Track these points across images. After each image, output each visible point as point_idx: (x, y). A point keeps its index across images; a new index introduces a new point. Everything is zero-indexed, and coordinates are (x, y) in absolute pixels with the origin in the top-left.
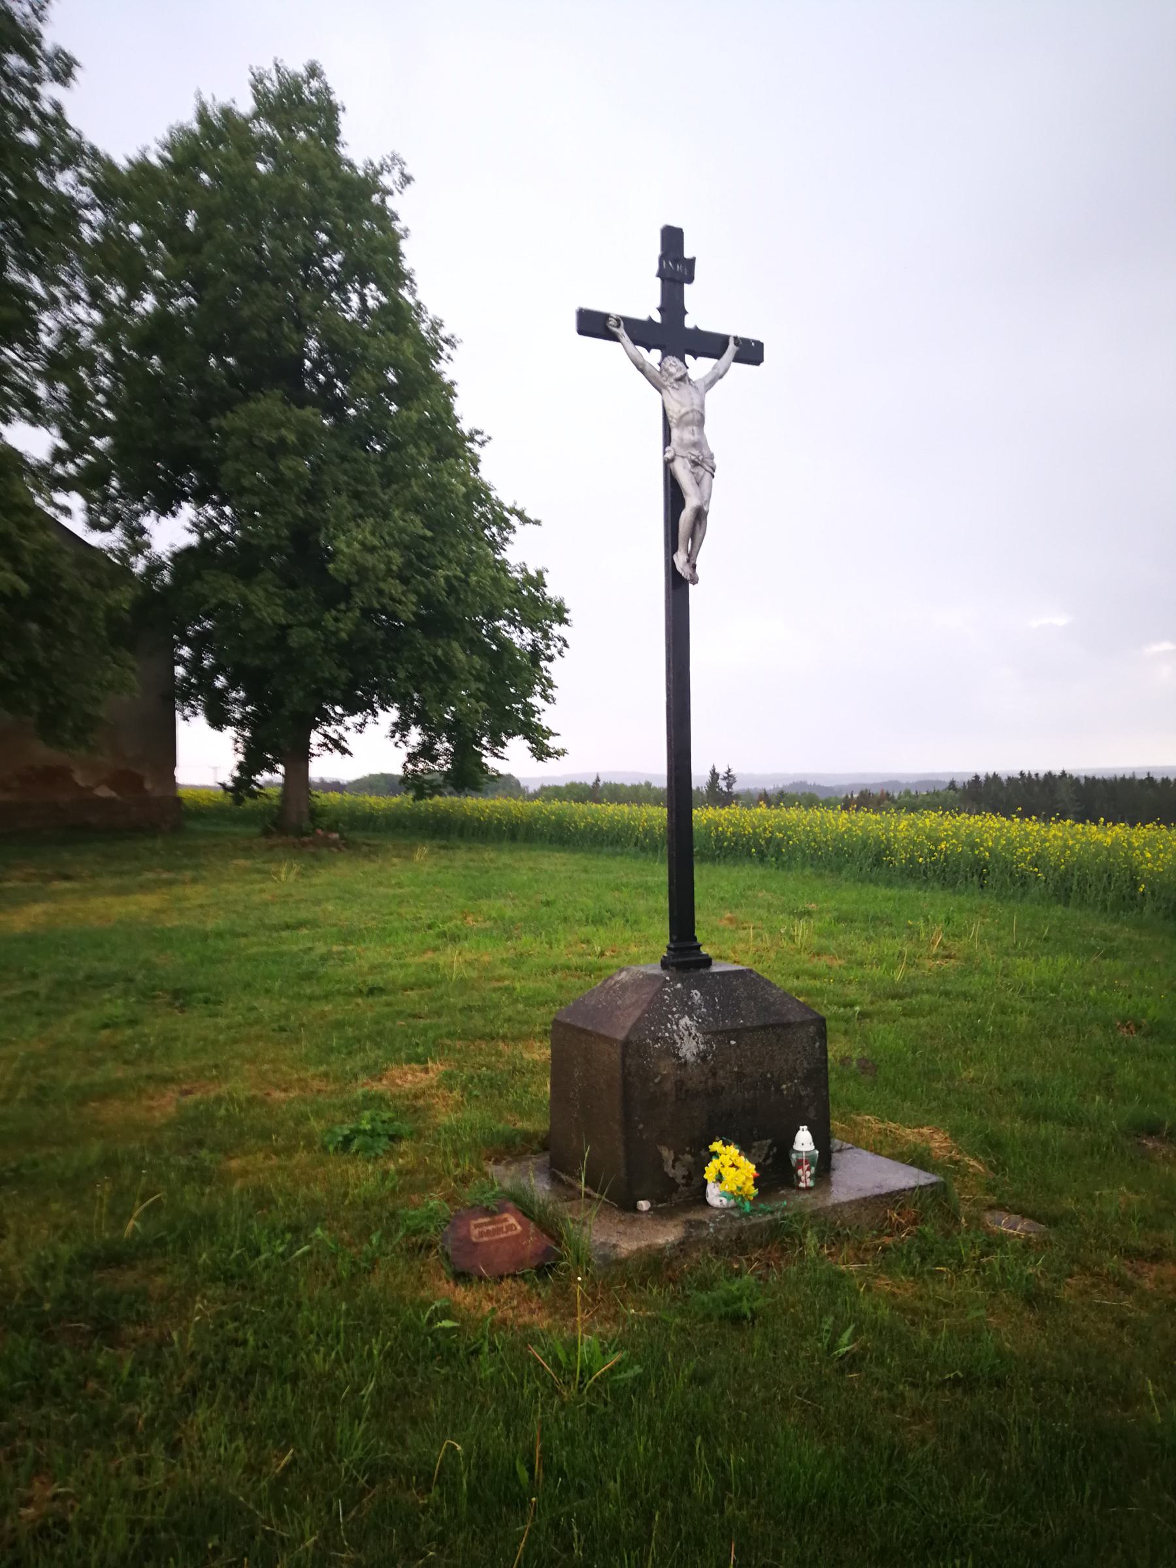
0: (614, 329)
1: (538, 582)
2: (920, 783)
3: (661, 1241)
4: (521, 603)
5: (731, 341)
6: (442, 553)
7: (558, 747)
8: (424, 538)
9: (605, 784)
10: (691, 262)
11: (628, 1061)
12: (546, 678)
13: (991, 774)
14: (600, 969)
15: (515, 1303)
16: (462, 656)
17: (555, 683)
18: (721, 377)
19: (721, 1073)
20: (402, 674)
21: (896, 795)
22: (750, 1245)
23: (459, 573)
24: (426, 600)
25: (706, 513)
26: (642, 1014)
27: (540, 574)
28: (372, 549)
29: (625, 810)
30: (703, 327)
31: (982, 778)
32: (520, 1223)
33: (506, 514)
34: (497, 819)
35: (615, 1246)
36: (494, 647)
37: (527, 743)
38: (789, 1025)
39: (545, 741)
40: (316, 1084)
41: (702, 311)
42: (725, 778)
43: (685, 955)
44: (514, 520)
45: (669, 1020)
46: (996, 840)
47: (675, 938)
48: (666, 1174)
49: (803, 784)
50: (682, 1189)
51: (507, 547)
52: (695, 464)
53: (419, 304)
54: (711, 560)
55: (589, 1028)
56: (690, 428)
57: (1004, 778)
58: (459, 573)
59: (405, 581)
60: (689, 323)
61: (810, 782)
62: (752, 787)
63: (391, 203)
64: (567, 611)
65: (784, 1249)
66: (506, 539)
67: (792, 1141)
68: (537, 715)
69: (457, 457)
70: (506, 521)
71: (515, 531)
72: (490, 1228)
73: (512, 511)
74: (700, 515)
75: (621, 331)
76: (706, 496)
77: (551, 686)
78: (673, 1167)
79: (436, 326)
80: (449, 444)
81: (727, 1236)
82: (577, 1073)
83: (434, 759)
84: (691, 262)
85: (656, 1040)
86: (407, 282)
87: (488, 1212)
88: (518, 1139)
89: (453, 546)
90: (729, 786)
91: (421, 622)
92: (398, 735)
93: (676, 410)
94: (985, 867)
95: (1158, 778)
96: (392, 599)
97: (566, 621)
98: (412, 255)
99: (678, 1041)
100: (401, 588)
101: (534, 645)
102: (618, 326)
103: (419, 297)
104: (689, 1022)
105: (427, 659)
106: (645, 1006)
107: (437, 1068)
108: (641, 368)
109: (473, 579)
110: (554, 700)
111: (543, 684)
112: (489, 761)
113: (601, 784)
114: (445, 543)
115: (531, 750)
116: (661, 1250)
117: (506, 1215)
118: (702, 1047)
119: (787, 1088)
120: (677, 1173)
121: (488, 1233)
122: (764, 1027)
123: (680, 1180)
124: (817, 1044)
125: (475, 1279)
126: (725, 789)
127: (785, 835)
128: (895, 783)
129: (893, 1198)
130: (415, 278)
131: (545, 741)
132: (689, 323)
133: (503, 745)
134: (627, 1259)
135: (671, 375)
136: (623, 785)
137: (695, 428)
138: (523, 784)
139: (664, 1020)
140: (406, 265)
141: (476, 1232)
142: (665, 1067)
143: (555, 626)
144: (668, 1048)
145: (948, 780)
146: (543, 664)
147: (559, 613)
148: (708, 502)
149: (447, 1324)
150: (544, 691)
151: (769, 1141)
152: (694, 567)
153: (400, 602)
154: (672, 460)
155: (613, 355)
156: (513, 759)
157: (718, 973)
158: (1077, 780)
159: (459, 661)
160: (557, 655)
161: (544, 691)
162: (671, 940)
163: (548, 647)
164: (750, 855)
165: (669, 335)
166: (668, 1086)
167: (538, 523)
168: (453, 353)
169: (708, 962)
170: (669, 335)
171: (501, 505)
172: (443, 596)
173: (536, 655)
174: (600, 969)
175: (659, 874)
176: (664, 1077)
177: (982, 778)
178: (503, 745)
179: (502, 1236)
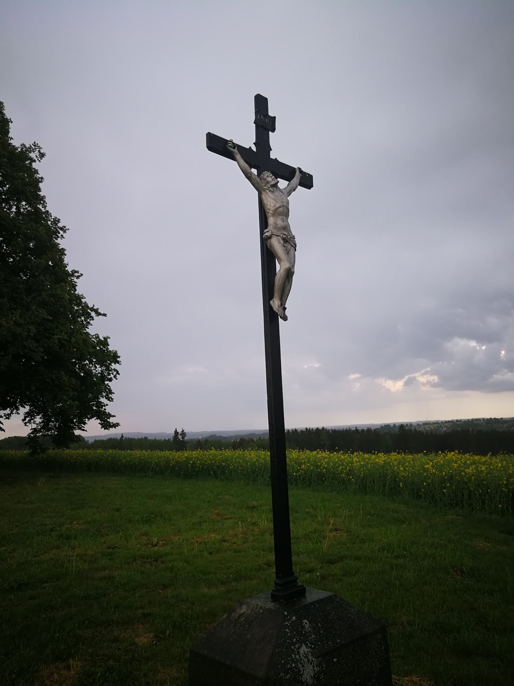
1: (105, 343)
4: (96, 354)
5: (298, 173)
8: (48, 320)
9: (126, 438)
12: (108, 389)
13: (294, 429)
14: (161, 556)
17: (113, 391)
18: (294, 190)
21: (255, 439)
23: (66, 337)
25: (293, 273)
27: (106, 339)
28: (20, 325)
29: (145, 453)
31: (291, 431)
36: (82, 374)
37: (99, 421)
39: (108, 420)
41: (281, 149)
42: (181, 435)
44: (93, 314)
51: (89, 327)
52: (285, 240)
53: (47, 211)
56: (281, 217)
57: (299, 431)
58: (66, 337)
60: (273, 156)
62: (192, 438)
63: (34, 165)
64: (119, 357)
66: (89, 323)
68: (104, 407)
69: (66, 283)
71: (93, 319)
73: (92, 309)
74: (289, 274)
76: (292, 261)
90: (183, 438)
92: (28, 419)
93: (272, 205)
94: (324, 476)
95: (360, 429)
97: (118, 362)
98: (45, 189)
101: (102, 373)
102: (234, 148)
103: (47, 209)
104: (306, 650)
105: (47, 380)
108: (249, 176)
109: (73, 340)
110: (112, 399)
111: (107, 392)
113: (124, 438)
115: (101, 424)
118: (316, 669)
126: (181, 439)
127: (226, 463)
130: (46, 200)
131: (108, 420)
132: (273, 155)
133: (85, 423)
135: (268, 182)
136: (134, 439)
137: (284, 218)
138: (86, 439)
143: (113, 364)
147: (115, 358)
152: (285, 309)
153: (35, 351)
154: (270, 237)
155: (231, 169)
156: (92, 429)
158: (329, 431)
160: (114, 379)
162: (277, 577)
163: (109, 374)
164: (210, 474)
167: (105, 315)
168: (65, 235)
169: (302, 592)
170: (259, 162)
171: (87, 306)
173: (103, 378)
174: (161, 556)
177: (291, 431)
178: (85, 423)
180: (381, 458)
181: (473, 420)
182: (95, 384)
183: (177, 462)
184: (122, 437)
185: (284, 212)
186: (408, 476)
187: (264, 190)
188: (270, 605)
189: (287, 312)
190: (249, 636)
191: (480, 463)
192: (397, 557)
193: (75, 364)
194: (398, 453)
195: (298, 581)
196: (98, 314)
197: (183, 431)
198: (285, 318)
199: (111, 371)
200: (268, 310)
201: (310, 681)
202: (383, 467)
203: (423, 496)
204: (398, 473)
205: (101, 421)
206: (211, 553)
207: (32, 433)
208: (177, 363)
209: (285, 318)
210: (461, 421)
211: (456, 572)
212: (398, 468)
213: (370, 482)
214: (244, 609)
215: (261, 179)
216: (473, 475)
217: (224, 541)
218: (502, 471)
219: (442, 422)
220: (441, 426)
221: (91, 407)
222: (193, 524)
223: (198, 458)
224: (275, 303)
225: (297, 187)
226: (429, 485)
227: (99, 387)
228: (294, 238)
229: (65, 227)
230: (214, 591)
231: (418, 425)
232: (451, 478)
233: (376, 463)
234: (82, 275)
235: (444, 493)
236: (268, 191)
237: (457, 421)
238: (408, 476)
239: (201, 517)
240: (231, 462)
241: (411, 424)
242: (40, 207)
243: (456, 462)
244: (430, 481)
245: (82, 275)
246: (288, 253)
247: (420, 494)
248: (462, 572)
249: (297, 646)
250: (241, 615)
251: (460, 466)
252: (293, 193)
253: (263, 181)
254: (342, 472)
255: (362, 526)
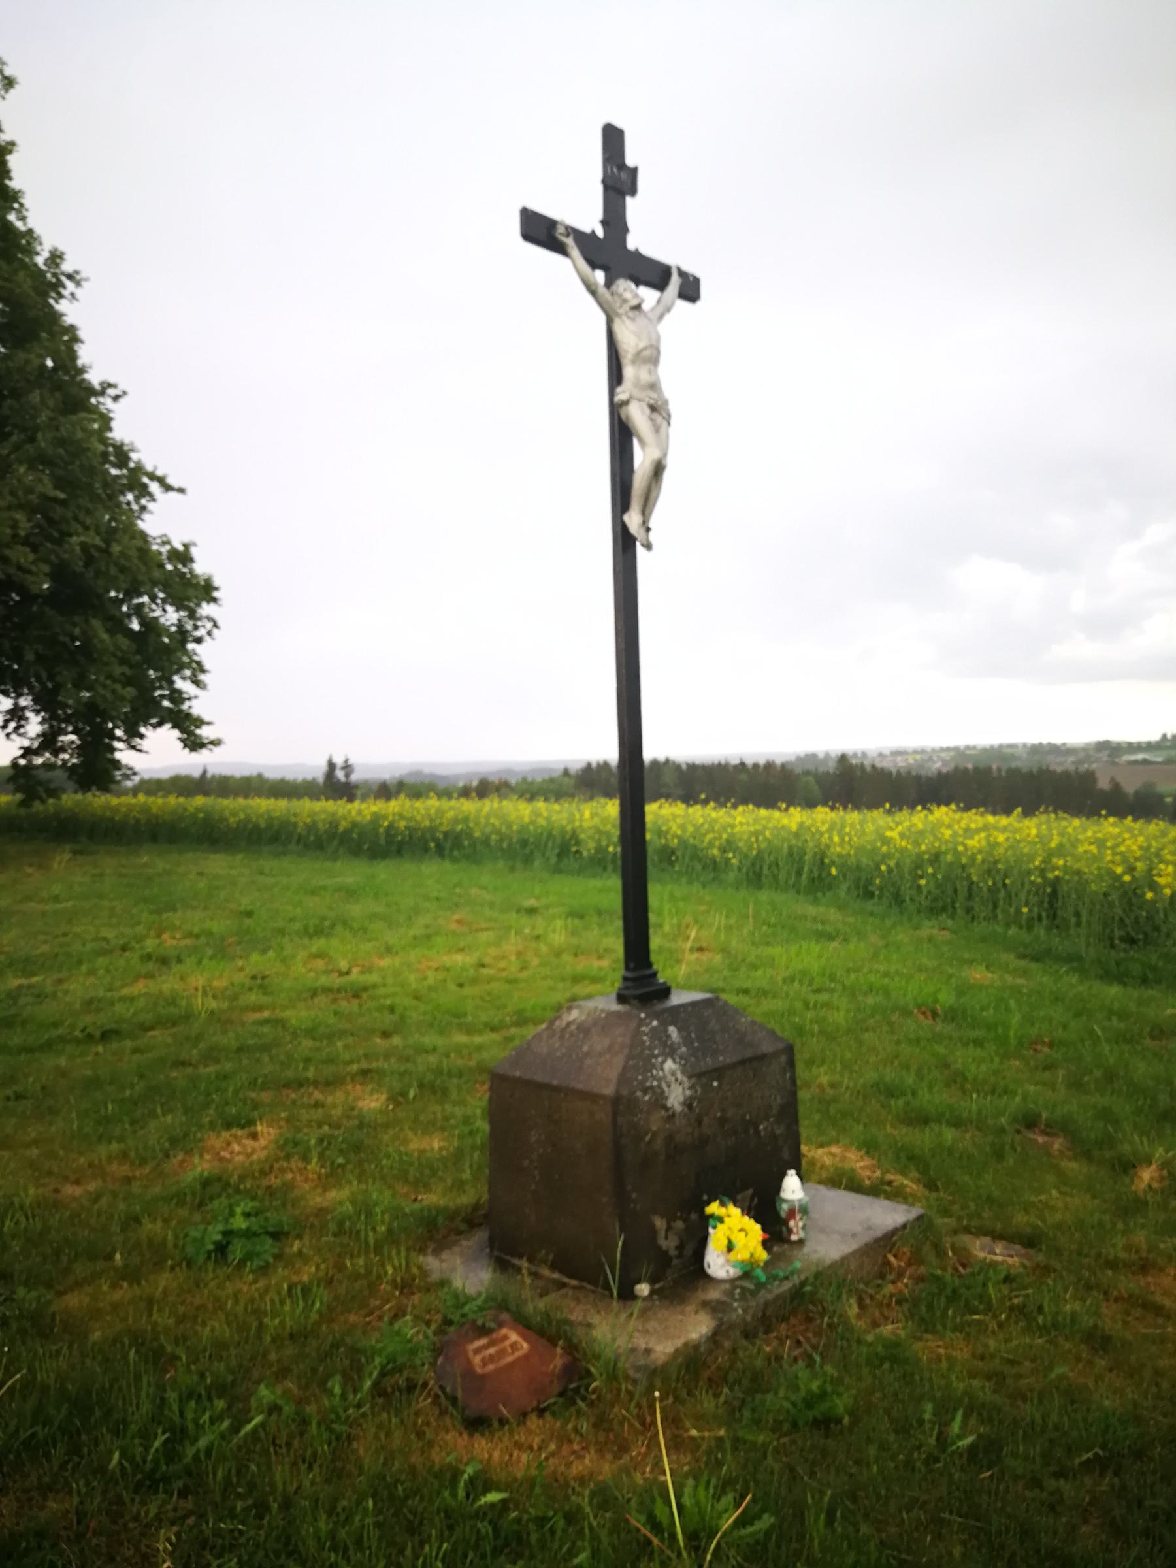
0: (563, 239)
1: (183, 556)
2: (533, 771)
3: (694, 1336)
6: (76, 519)
7: (213, 737)
8: (55, 500)
9: (213, 776)
10: (634, 171)
11: (620, 1120)
13: (601, 762)
15: (553, 1447)
16: (105, 636)
19: (706, 1120)
20: (30, 656)
22: (774, 1320)
23: (98, 541)
24: (60, 573)
26: (626, 1062)
27: (186, 546)
30: (647, 251)
32: (525, 1339)
33: (145, 480)
34: (134, 817)
35: (648, 1351)
37: (176, 733)
38: (762, 1058)
40: (119, 1169)
41: (644, 236)
43: (642, 985)
44: (154, 487)
45: (654, 1066)
46: (683, 827)
47: (632, 965)
48: (660, 1248)
49: (418, 773)
50: (675, 1262)
52: (653, 408)
54: (667, 522)
55: (555, 1082)
57: (594, 765)
59: (35, 548)
61: (426, 771)
64: (216, 589)
65: (809, 1320)
67: (778, 1187)
70: (145, 486)
72: (492, 1351)
73: (152, 477)
74: (658, 469)
75: (570, 241)
77: (203, 671)
78: (666, 1238)
79: (56, 258)
80: (76, 397)
81: (753, 1317)
82: (534, 1137)
83: (56, 752)
84: (634, 171)
85: (645, 1091)
86: (16, 206)
87: (483, 1331)
88: (440, 1220)
89: (89, 512)
90: (347, 775)
91: (51, 598)
92: (12, 725)
95: (749, 762)
96: (20, 568)
97: (215, 600)
99: (666, 1089)
100: (31, 557)
101: (180, 625)
102: (568, 235)
106: (626, 1051)
107: (267, 1133)
108: (592, 291)
109: (116, 549)
112: (124, 755)
114: (79, 507)
115: (181, 739)
116: (696, 1347)
117: (504, 1331)
119: (765, 1129)
120: (668, 1244)
121: (492, 1359)
122: (743, 1062)
123: (673, 1253)
124: (788, 1075)
125: (496, 1424)
128: (509, 771)
129: (888, 1241)
131: (198, 732)
132: (632, 243)
134: (666, 1365)
135: (625, 301)
139: (648, 1066)
140: (14, 184)
141: (477, 1360)
142: (655, 1123)
143: (204, 604)
144: (656, 1100)
145: (561, 767)
146: (191, 646)
147: (207, 591)
148: (665, 455)
149: (493, 1497)
150: (194, 675)
151: (750, 1191)
152: (648, 530)
153: (30, 572)
154: (626, 403)
155: (562, 272)
156: (155, 754)
157: (683, 1006)
159: (102, 641)
161: (194, 675)
162: (627, 968)
163: (196, 628)
165: (609, 255)
166: (659, 1143)
167: (181, 490)
168: (79, 292)
169: (665, 992)
170: (609, 255)
172: (79, 565)
173: (182, 636)
175: (608, 891)
176: (654, 1134)
179: (510, 1359)
180: (793, 818)
181: (1001, 746)
182: (167, 650)
183: (355, 824)
184: (205, 772)
185: (651, 356)
186: (849, 855)
187: (618, 315)
188: (615, 1007)
189: (652, 536)
190: (585, 1049)
191: (996, 828)
192: (818, 991)
193: (118, 602)
194: (833, 808)
195: (659, 975)
196: (168, 488)
197: (346, 761)
198: (648, 546)
199: (199, 619)
200: (619, 534)
201: (678, 1108)
202: (797, 835)
203: (877, 893)
204: (828, 847)
205: (182, 732)
206: (461, 985)
207: (23, 756)
208: (368, 603)
209: (648, 546)
210: (975, 748)
211: (924, 1013)
212: (831, 838)
213: (770, 867)
214: (575, 1014)
215: (612, 294)
216: (980, 852)
217: (483, 966)
218: (1037, 843)
219: (933, 750)
220: (931, 759)
221: (156, 703)
222: (415, 938)
223: (402, 817)
224: (633, 520)
225: (673, 304)
226: (890, 870)
227: (168, 655)
228: (666, 402)
229: (77, 272)
230: (478, 1040)
231: (881, 755)
232: (936, 858)
233: (783, 828)
234: (125, 393)
235: (919, 887)
236: (625, 318)
237: (968, 747)
238: (849, 855)
239: (427, 927)
240: (477, 824)
241: (864, 754)
242: (12, 217)
243: (949, 827)
244: (892, 863)
245: (125, 393)
246: (657, 429)
247: (871, 888)
248: (935, 1014)
249: (660, 1059)
250: (569, 1024)
251: (955, 834)
252: (667, 317)
253: (616, 298)
254: (711, 845)
255: (753, 943)
